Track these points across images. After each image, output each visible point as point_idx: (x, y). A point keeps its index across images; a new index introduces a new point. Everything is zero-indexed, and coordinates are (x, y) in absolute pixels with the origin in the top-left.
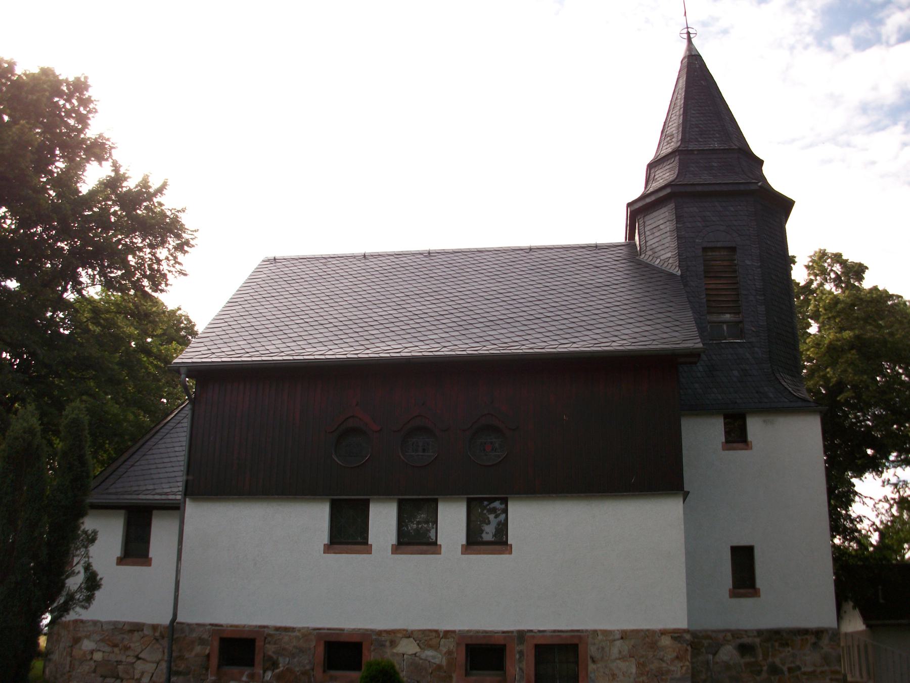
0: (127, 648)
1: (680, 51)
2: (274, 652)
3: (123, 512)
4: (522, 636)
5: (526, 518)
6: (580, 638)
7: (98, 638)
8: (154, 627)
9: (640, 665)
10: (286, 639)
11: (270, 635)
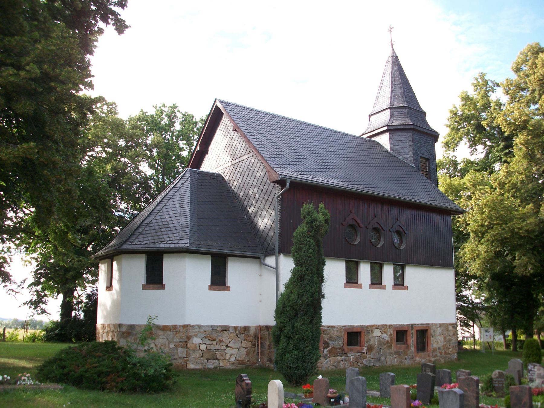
0: (221, 341)
1: (389, 53)
2: (328, 339)
3: (210, 257)
4: (412, 326)
5: (412, 274)
6: (428, 327)
7: (203, 336)
8: (235, 328)
9: (445, 338)
10: (332, 332)
11: (325, 330)
